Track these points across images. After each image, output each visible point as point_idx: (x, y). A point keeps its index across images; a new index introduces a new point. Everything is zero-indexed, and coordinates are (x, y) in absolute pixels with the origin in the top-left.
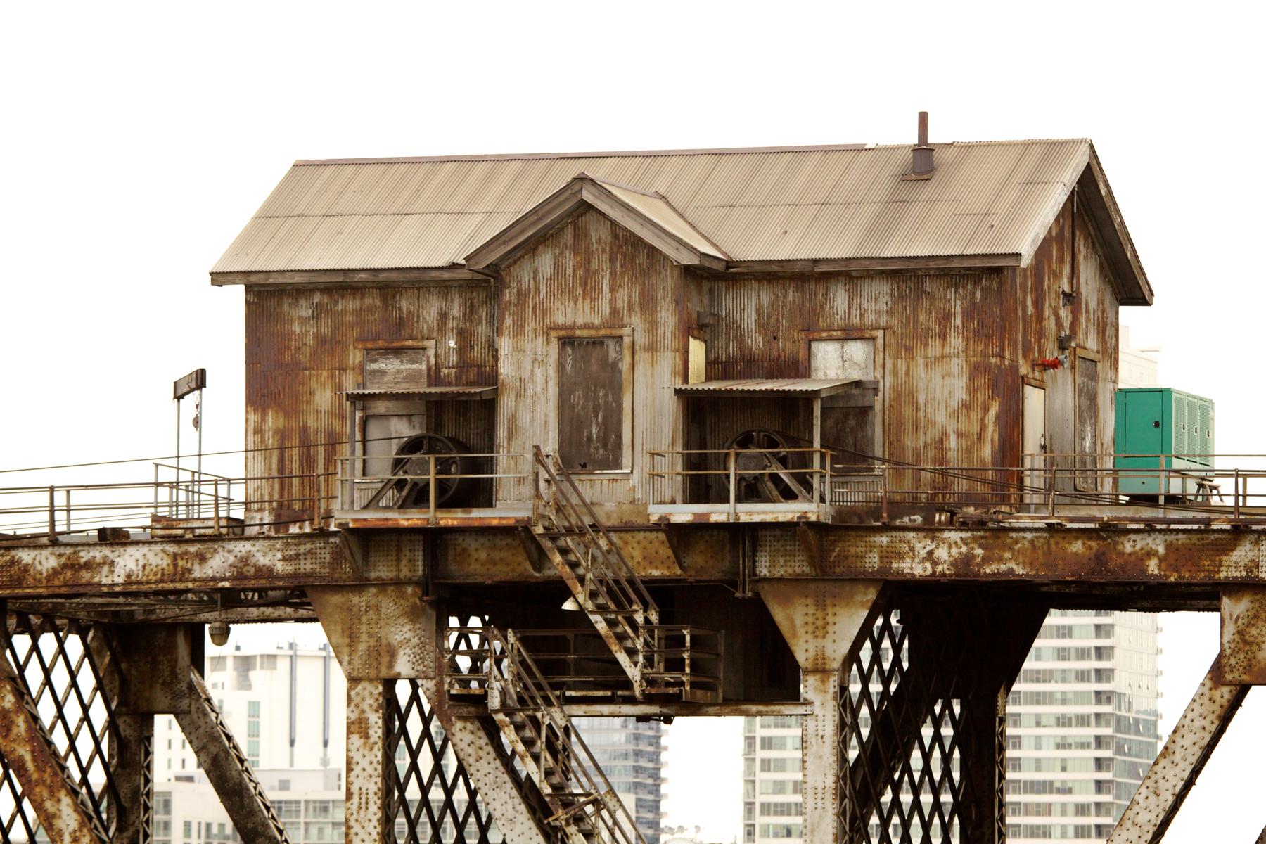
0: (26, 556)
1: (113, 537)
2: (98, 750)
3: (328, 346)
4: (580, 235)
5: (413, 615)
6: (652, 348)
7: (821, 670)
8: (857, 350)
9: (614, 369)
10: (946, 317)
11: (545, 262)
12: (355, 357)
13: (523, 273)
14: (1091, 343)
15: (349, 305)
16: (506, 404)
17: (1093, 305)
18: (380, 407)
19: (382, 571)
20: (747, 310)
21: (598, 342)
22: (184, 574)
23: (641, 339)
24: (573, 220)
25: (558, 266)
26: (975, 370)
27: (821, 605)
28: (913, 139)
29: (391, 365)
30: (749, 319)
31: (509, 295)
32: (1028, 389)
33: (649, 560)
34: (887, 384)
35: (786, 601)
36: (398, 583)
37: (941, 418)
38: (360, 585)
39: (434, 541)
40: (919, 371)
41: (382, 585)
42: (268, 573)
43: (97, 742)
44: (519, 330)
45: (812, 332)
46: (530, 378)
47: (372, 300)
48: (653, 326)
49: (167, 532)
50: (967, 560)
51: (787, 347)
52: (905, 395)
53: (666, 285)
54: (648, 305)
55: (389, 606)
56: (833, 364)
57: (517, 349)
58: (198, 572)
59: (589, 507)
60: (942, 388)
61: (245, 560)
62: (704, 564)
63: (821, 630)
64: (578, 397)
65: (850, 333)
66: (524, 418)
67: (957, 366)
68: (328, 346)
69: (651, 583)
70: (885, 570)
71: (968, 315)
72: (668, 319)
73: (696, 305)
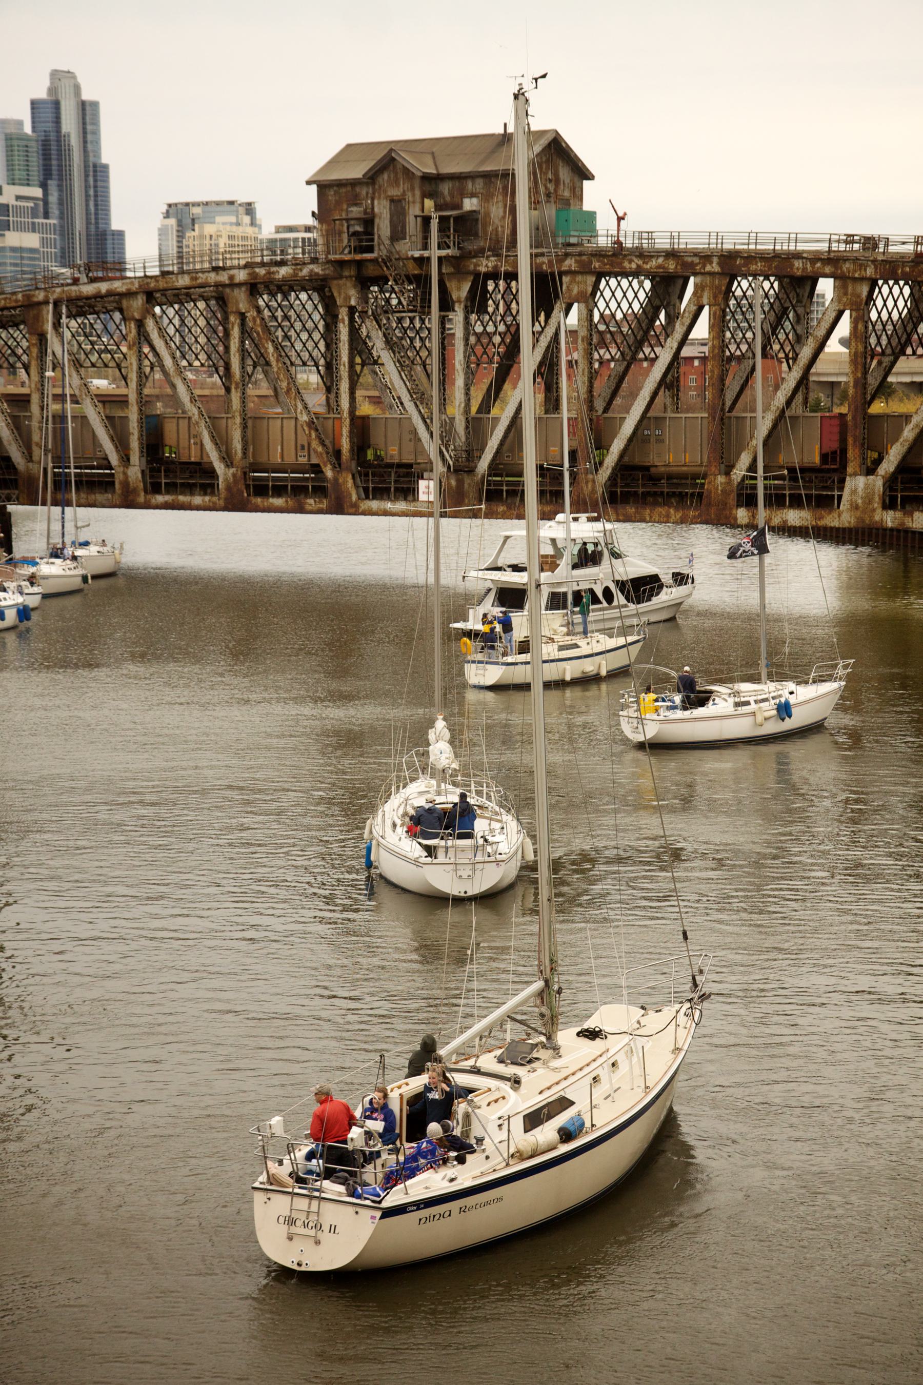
0: (257, 270)
2: (906, 305)
3: (338, 203)
4: (395, 167)
5: (355, 287)
6: (414, 202)
7: (459, 301)
8: (475, 200)
9: (404, 209)
11: (385, 176)
12: (345, 207)
14: (567, 194)
15: (343, 190)
16: (377, 221)
17: (567, 181)
18: (352, 222)
19: (346, 273)
21: (400, 201)
22: (296, 275)
28: (502, 132)
29: (354, 209)
30: (446, 192)
34: (482, 211)
35: (450, 280)
36: (350, 277)
37: (497, 221)
38: (341, 277)
39: (359, 264)
42: (317, 274)
43: (906, 302)
44: (379, 198)
45: (463, 195)
46: (382, 209)
48: (414, 195)
51: (457, 200)
52: (487, 214)
53: (417, 183)
54: (413, 189)
55: (349, 284)
56: (469, 204)
58: (300, 274)
59: (398, 253)
63: (459, 289)
64: (395, 218)
65: (472, 195)
66: (381, 225)
68: (338, 203)
72: (418, 193)
73: (428, 188)
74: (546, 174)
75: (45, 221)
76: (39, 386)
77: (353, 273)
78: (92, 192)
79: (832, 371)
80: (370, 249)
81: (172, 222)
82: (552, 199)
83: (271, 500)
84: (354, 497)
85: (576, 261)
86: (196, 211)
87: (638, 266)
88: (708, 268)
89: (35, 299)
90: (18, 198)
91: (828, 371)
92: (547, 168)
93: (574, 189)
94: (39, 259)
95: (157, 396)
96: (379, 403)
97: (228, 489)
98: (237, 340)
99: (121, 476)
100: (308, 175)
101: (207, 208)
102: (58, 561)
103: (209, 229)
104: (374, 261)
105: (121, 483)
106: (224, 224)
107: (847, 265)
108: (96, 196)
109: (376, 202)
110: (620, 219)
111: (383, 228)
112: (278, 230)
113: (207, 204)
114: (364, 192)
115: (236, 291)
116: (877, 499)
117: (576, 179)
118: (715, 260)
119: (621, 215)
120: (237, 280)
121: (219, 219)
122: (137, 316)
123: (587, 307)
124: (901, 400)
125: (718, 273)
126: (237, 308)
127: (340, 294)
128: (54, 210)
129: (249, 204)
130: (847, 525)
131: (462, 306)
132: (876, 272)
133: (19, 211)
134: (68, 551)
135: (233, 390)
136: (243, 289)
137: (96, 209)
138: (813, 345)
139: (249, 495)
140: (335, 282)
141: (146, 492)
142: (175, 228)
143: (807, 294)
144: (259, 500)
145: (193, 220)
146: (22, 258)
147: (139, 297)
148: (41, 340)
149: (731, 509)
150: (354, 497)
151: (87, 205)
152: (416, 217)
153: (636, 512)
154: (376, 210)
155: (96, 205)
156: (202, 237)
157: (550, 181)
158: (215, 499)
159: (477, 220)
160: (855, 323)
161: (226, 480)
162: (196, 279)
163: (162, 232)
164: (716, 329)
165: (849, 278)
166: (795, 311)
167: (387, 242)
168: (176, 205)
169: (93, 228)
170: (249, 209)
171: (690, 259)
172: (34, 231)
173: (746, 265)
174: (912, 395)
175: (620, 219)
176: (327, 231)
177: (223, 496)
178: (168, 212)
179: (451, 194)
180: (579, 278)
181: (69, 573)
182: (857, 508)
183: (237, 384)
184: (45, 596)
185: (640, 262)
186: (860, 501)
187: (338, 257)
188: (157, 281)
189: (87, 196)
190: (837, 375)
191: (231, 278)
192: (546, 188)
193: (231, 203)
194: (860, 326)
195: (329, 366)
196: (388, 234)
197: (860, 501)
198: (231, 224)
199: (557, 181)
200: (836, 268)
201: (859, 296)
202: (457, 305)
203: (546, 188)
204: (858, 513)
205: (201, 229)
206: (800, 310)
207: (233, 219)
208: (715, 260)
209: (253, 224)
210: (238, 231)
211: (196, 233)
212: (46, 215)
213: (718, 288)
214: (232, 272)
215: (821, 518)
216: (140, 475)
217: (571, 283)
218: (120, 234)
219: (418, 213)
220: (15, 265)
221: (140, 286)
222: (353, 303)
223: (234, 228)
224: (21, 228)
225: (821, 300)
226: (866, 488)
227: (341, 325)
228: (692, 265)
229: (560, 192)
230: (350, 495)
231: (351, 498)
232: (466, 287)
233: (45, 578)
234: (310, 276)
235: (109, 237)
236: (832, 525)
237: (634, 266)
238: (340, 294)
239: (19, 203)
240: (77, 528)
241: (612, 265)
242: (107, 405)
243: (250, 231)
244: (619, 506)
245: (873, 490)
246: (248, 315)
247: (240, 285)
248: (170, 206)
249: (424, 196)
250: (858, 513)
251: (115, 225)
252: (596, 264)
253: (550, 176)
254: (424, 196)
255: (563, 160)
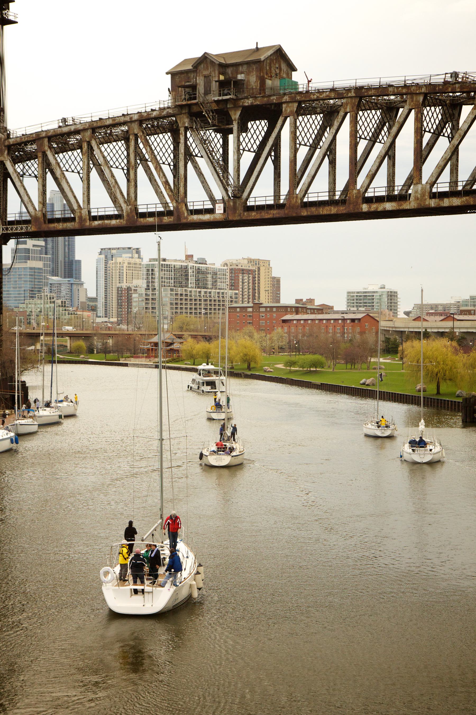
1: (152, 110)
4: (206, 61)
5: (187, 117)
6: (215, 77)
7: (235, 120)
8: (243, 75)
9: (210, 80)
10: (253, 69)
11: (202, 66)
13: (200, 68)
15: (183, 76)
16: (198, 86)
17: (285, 70)
19: (184, 112)
20: (229, 71)
21: (208, 76)
22: (161, 114)
23: (214, 75)
24: (205, 59)
25: (204, 66)
26: (257, 76)
27: (235, 111)
30: (230, 72)
31: (198, 71)
32: (267, 80)
33: (215, 107)
36: (186, 113)
38: (181, 114)
39: (189, 106)
40: (250, 78)
41: (184, 113)
42: (170, 113)
44: (199, 76)
45: (237, 73)
46: (200, 81)
47: (185, 75)
48: (215, 73)
49: (160, 109)
50: (252, 103)
52: (248, 81)
53: (217, 68)
54: (214, 71)
55: (185, 117)
56: (240, 77)
57: (199, 79)
59: (207, 100)
60: (253, 80)
61: (168, 112)
62: (221, 106)
63: (235, 114)
65: (242, 73)
66: (200, 88)
67: (255, 76)
69: (215, 110)
70: (243, 105)
71: (256, 69)
73: (221, 70)
74: (275, 65)
75: (45, 256)
76: (42, 176)
77: (187, 111)
78: (67, 243)
79: (402, 326)
80: (195, 98)
81: (103, 256)
82: (278, 77)
83: (147, 219)
84: (186, 214)
85: (289, 97)
86: (114, 252)
87: (317, 97)
88: (350, 95)
89: (41, 136)
90: (34, 246)
91: (400, 326)
92: (276, 62)
93: (288, 74)
94: (42, 273)
95: (95, 334)
96: (196, 338)
97: (128, 215)
98: (133, 147)
99: (79, 214)
100: (168, 70)
101: (118, 251)
102: (48, 409)
103: (119, 260)
104: (196, 104)
105: (78, 217)
106: (126, 257)
107: (413, 88)
108: (69, 245)
109: (198, 78)
110: (309, 81)
111: (201, 89)
112: (151, 260)
113: (119, 248)
114: (192, 76)
115: (133, 124)
116: (427, 194)
117: (289, 70)
118: (353, 91)
119: (309, 80)
120: (133, 119)
121: (123, 255)
122: (87, 140)
123: (294, 117)
124: (434, 340)
125: (354, 97)
126: (134, 132)
127: (180, 121)
128: (50, 251)
129: (138, 249)
130: (413, 207)
131: (237, 122)
132: (426, 90)
133: (34, 251)
134: (53, 404)
135: (131, 170)
136: (136, 123)
137: (69, 251)
138: (397, 126)
139: (137, 218)
140: (179, 116)
141: (90, 220)
142: (104, 259)
143: (394, 116)
144: (142, 219)
145: (112, 256)
146: (35, 272)
147: (89, 131)
148: (43, 155)
149: (360, 205)
150: (186, 214)
151: (65, 249)
152: (216, 81)
153: (316, 210)
154: (198, 81)
155: (69, 249)
156: (116, 263)
157: (277, 68)
158: (122, 221)
159: (244, 84)
160: (417, 114)
161: (127, 211)
162: (115, 120)
163: (98, 261)
164: (353, 123)
165: (414, 93)
166: (389, 123)
167: (203, 96)
168: (105, 249)
169: (67, 259)
170: (138, 251)
171: (341, 92)
172: (40, 260)
173: (367, 92)
174: (438, 338)
175: (309, 81)
176: (175, 95)
177: (125, 219)
178: (101, 252)
179: (232, 73)
180: (290, 105)
181: (52, 414)
182: (418, 199)
183: (133, 167)
184: (40, 426)
185: (318, 95)
186: (419, 196)
187: (180, 103)
188: (97, 123)
189: (65, 245)
190: (404, 328)
191: (131, 118)
192: (275, 71)
193: (130, 248)
194: (419, 115)
195: (175, 166)
196: (203, 92)
197: (419, 196)
198: (130, 257)
199: (280, 69)
200: (408, 89)
201: (419, 101)
202: (234, 122)
203: (275, 71)
204: (418, 202)
205: (116, 259)
206: (391, 123)
207: (130, 255)
208: (353, 91)
209: (139, 257)
210: (132, 261)
211: (113, 261)
212: (46, 254)
213: (354, 104)
214: (131, 116)
215: (401, 205)
216: (87, 213)
217: (287, 107)
218: (79, 262)
219: (216, 79)
220: (32, 281)
221: (89, 126)
222: (186, 125)
223: (131, 259)
224: (34, 259)
225: (395, 294)
226: (422, 190)
227: (181, 136)
228: (342, 94)
229: (282, 74)
230: (184, 214)
231: (184, 214)
232: (239, 113)
233: (40, 417)
234: (167, 114)
235: (74, 263)
236: (406, 208)
237: (315, 97)
238: (180, 121)
239: (34, 248)
240: (57, 394)
241: (305, 97)
242: (72, 338)
243: (138, 261)
244: (308, 208)
245: (425, 190)
246: (138, 135)
247: (135, 121)
248: (102, 249)
249: (220, 73)
250: (418, 202)
251: (77, 258)
252: (298, 98)
253: (277, 66)
254: (220, 73)
255: (283, 60)
